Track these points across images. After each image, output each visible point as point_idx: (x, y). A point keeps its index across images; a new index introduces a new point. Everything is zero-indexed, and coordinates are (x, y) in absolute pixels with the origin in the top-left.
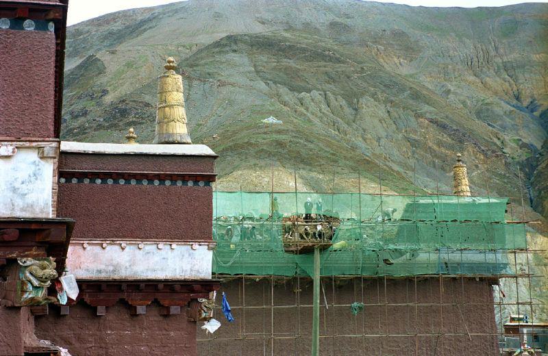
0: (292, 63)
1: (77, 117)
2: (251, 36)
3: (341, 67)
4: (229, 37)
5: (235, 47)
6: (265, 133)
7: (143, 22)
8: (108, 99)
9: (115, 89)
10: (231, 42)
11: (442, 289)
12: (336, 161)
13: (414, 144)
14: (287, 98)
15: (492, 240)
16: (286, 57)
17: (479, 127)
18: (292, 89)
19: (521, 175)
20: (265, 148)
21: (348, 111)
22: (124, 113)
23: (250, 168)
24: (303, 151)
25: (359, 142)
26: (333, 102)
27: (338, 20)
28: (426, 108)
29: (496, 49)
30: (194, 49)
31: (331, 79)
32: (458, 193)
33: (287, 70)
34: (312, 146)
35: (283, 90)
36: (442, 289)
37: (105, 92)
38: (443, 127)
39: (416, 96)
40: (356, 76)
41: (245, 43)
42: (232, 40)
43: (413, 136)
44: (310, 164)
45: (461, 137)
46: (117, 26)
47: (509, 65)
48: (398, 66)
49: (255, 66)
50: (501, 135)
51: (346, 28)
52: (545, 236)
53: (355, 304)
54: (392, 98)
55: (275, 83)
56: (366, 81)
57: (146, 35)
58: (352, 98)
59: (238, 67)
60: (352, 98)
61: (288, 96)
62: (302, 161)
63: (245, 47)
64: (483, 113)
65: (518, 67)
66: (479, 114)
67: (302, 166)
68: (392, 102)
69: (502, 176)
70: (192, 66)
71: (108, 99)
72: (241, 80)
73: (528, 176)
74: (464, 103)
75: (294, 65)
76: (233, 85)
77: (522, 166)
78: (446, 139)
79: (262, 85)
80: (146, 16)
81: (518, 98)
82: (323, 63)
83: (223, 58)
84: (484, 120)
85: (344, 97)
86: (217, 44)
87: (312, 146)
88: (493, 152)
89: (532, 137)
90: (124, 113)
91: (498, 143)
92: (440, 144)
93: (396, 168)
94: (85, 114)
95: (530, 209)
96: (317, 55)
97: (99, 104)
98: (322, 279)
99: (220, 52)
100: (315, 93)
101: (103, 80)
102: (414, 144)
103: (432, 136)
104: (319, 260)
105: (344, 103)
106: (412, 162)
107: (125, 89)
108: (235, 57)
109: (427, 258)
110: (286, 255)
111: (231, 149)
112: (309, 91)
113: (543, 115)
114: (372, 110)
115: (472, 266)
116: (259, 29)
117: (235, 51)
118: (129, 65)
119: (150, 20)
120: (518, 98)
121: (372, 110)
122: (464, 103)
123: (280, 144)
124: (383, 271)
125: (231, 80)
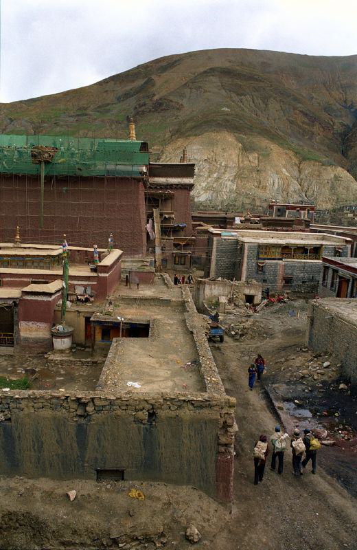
0: (239, 82)
2: (221, 69)
3: (262, 84)
4: (211, 69)
7: (176, 62)
13: (291, 122)
17: (324, 116)
18: (238, 94)
19: (340, 139)
21: (263, 105)
22: (161, 104)
25: (265, 121)
26: (256, 101)
27: (265, 61)
28: (299, 105)
29: (339, 77)
31: (256, 90)
34: (241, 122)
35: (233, 95)
37: (154, 95)
38: (306, 115)
39: (295, 99)
40: (268, 88)
41: (218, 72)
42: (212, 70)
43: (290, 118)
45: (313, 120)
46: (164, 64)
48: (291, 85)
49: (222, 83)
50: (333, 120)
54: (284, 100)
55: (230, 91)
58: (265, 100)
59: (214, 83)
60: (265, 100)
61: (236, 98)
62: (236, 129)
63: (216, 73)
64: (327, 109)
65: (348, 87)
66: (325, 109)
67: (235, 131)
69: (329, 139)
72: (216, 90)
73: (343, 140)
74: (319, 104)
75: (239, 83)
76: (210, 92)
77: (341, 135)
78: (306, 120)
79: (223, 92)
81: (345, 102)
82: (252, 82)
84: (327, 112)
86: (205, 72)
87: (241, 122)
88: (326, 127)
89: (348, 121)
90: (161, 104)
91: (332, 123)
92: (303, 123)
93: (280, 133)
94: (145, 105)
95: (341, 155)
96: (251, 78)
97: (151, 100)
98: (46, 177)
102: (291, 122)
103: (301, 119)
104: (44, 167)
105: (261, 101)
106: (289, 131)
107: (163, 93)
109: (100, 167)
110: (33, 165)
111: (205, 122)
113: (355, 112)
114: (274, 106)
116: (228, 65)
117: (213, 76)
119: (179, 60)
120: (345, 102)
121: (274, 106)
122: (319, 104)
123: (228, 121)
124: (79, 173)
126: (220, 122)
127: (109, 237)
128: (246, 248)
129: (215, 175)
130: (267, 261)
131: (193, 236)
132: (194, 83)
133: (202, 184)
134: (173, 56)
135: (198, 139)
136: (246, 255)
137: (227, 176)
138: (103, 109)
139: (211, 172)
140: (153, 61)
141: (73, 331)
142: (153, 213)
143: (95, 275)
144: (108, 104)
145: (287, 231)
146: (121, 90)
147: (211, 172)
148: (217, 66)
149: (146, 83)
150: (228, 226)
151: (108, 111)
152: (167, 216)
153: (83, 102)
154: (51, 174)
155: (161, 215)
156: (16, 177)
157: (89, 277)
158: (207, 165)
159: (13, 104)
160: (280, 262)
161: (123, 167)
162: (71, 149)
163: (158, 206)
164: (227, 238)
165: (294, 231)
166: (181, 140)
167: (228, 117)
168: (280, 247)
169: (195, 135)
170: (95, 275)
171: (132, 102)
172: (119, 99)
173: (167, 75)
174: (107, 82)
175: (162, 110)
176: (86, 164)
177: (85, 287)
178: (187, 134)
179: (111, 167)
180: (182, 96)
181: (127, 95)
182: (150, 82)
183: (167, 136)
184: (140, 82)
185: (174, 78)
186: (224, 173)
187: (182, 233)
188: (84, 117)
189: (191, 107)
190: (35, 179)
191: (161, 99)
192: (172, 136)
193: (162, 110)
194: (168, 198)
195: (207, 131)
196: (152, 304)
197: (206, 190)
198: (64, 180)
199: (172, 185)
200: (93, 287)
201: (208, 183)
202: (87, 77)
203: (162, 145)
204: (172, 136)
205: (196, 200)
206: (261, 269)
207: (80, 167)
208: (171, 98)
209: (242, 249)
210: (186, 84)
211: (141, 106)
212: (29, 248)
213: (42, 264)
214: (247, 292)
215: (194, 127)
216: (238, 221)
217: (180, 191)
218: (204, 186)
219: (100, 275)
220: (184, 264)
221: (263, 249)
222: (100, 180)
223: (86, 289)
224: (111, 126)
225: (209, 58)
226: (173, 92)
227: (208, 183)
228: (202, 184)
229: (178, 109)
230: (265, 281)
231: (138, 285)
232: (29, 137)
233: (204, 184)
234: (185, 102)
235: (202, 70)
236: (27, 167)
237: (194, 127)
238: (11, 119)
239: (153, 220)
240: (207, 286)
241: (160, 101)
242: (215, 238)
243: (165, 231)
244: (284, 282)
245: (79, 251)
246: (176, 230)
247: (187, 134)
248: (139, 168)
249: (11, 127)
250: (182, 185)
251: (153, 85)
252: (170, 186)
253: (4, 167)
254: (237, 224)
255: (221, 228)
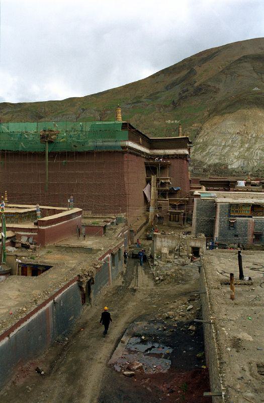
1: (185, 92)
4: (244, 56)
5: (246, 60)
6: (252, 94)
8: (196, 85)
9: (199, 81)
10: (245, 58)
11: (95, 156)
15: (115, 137)
22: (200, 89)
23: (244, 109)
30: (232, 62)
36: (95, 156)
37: (195, 82)
46: (205, 56)
49: (253, 67)
53: (64, 161)
57: (215, 58)
70: (228, 69)
71: (196, 85)
79: (255, 75)
80: (217, 50)
83: (241, 64)
86: (240, 59)
90: (200, 89)
94: (188, 91)
99: (239, 63)
101: (195, 77)
108: (246, 64)
109: (91, 144)
115: (106, 147)
117: (246, 62)
118: (205, 71)
124: (74, 149)
126: (251, 100)
127: (70, 198)
128: (218, 207)
129: (247, 146)
130: (237, 218)
131: (187, 198)
132: (229, 70)
133: (235, 153)
134: (212, 49)
135: (232, 116)
136: (218, 213)
137: (257, 146)
138: (153, 96)
139: (243, 143)
140: (196, 55)
141: (11, 270)
142: (151, 179)
143: (36, 227)
144: (158, 92)
145: (218, 190)
146: (169, 80)
147: (243, 143)
148: (250, 54)
149: (189, 73)
150: (231, 189)
151: (157, 98)
152: (163, 181)
153: (139, 93)
154: (54, 151)
155: (158, 180)
156: (110, 152)
157: (32, 229)
158: (240, 138)
159: (86, 97)
160: (250, 219)
161: (111, 143)
162: (63, 130)
163: (155, 173)
164: (205, 198)
165: (236, 191)
166: (217, 117)
168: (250, 206)
169: (229, 113)
170: (36, 227)
171: (177, 89)
172: (167, 88)
173: (206, 66)
174: (159, 75)
175: (202, 94)
176: (79, 142)
177: (29, 237)
178: (223, 112)
179: (99, 144)
180: (219, 81)
181: (173, 84)
182: (192, 72)
183: (205, 115)
184: (184, 73)
185: (214, 67)
186: (255, 143)
187: (178, 195)
188: (139, 104)
189: (225, 90)
190: (42, 155)
191: (200, 85)
192: (209, 115)
193: (202, 94)
194: (164, 167)
195: (239, 109)
196: (78, 251)
197: (238, 158)
198: (64, 155)
199: (168, 155)
200: (34, 237)
201: (240, 152)
202: (145, 72)
203: (201, 122)
204: (209, 115)
205: (229, 167)
206: (232, 225)
207: (75, 144)
208: (209, 83)
209: (216, 207)
210: (222, 71)
211: (184, 92)
212: (13, 207)
213: (12, 219)
214: (193, 244)
215: (228, 106)
216: (242, 184)
217: (176, 160)
218: (237, 155)
219: (40, 227)
220: (178, 221)
221: (234, 208)
222: (89, 154)
223: (28, 238)
224: (159, 110)
225: (243, 48)
226: (211, 78)
227: (240, 152)
228: (235, 153)
229: (215, 92)
230: (236, 236)
231: (84, 236)
232: (39, 123)
233: (236, 154)
234: (221, 86)
235: (236, 58)
236: (38, 147)
237: (228, 106)
238: (83, 110)
239: (151, 184)
240: (158, 238)
241: (200, 87)
242: (195, 199)
243: (162, 194)
244: (254, 237)
245: (49, 209)
246: (172, 193)
247: (223, 112)
248: (122, 143)
249: (83, 115)
250: (177, 155)
251: (195, 74)
252: (167, 157)
253: (22, 147)
254: (241, 187)
255: (226, 190)
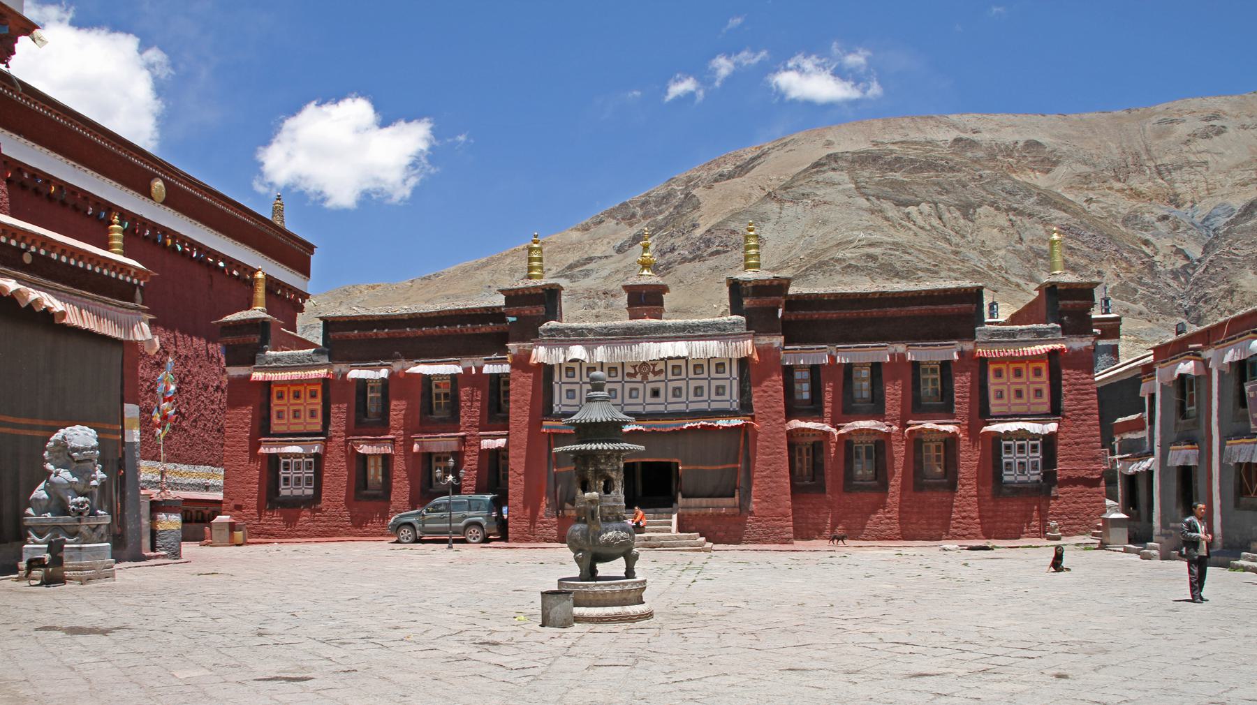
5: (834, 165)
12: (936, 273)
14: (890, 214)
16: (892, 170)
18: (900, 204)
20: (852, 262)
24: (898, 265)
26: (946, 216)
27: (964, 136)
32: (1149, 473)
33: (893, 184)
35: (887, 205)
40: (972, 185)
44: (906, 278)
47: (1162, 168)
49: (856, 183)
51: (972, 144)
52: (430, 141)
54: (1016, 206)
55: (878, 198)
56: (984, 189)
61: (892, 211)
68: (1015, 210)
72: (841, 198)
79: (862, 202)
85: (959, 208)
87: (909, 258)
100: (925, 207)
105: (957, 214)
112: (918, 204)
117: (834, 169)
125: (827, 199)
167: (871, 250)
